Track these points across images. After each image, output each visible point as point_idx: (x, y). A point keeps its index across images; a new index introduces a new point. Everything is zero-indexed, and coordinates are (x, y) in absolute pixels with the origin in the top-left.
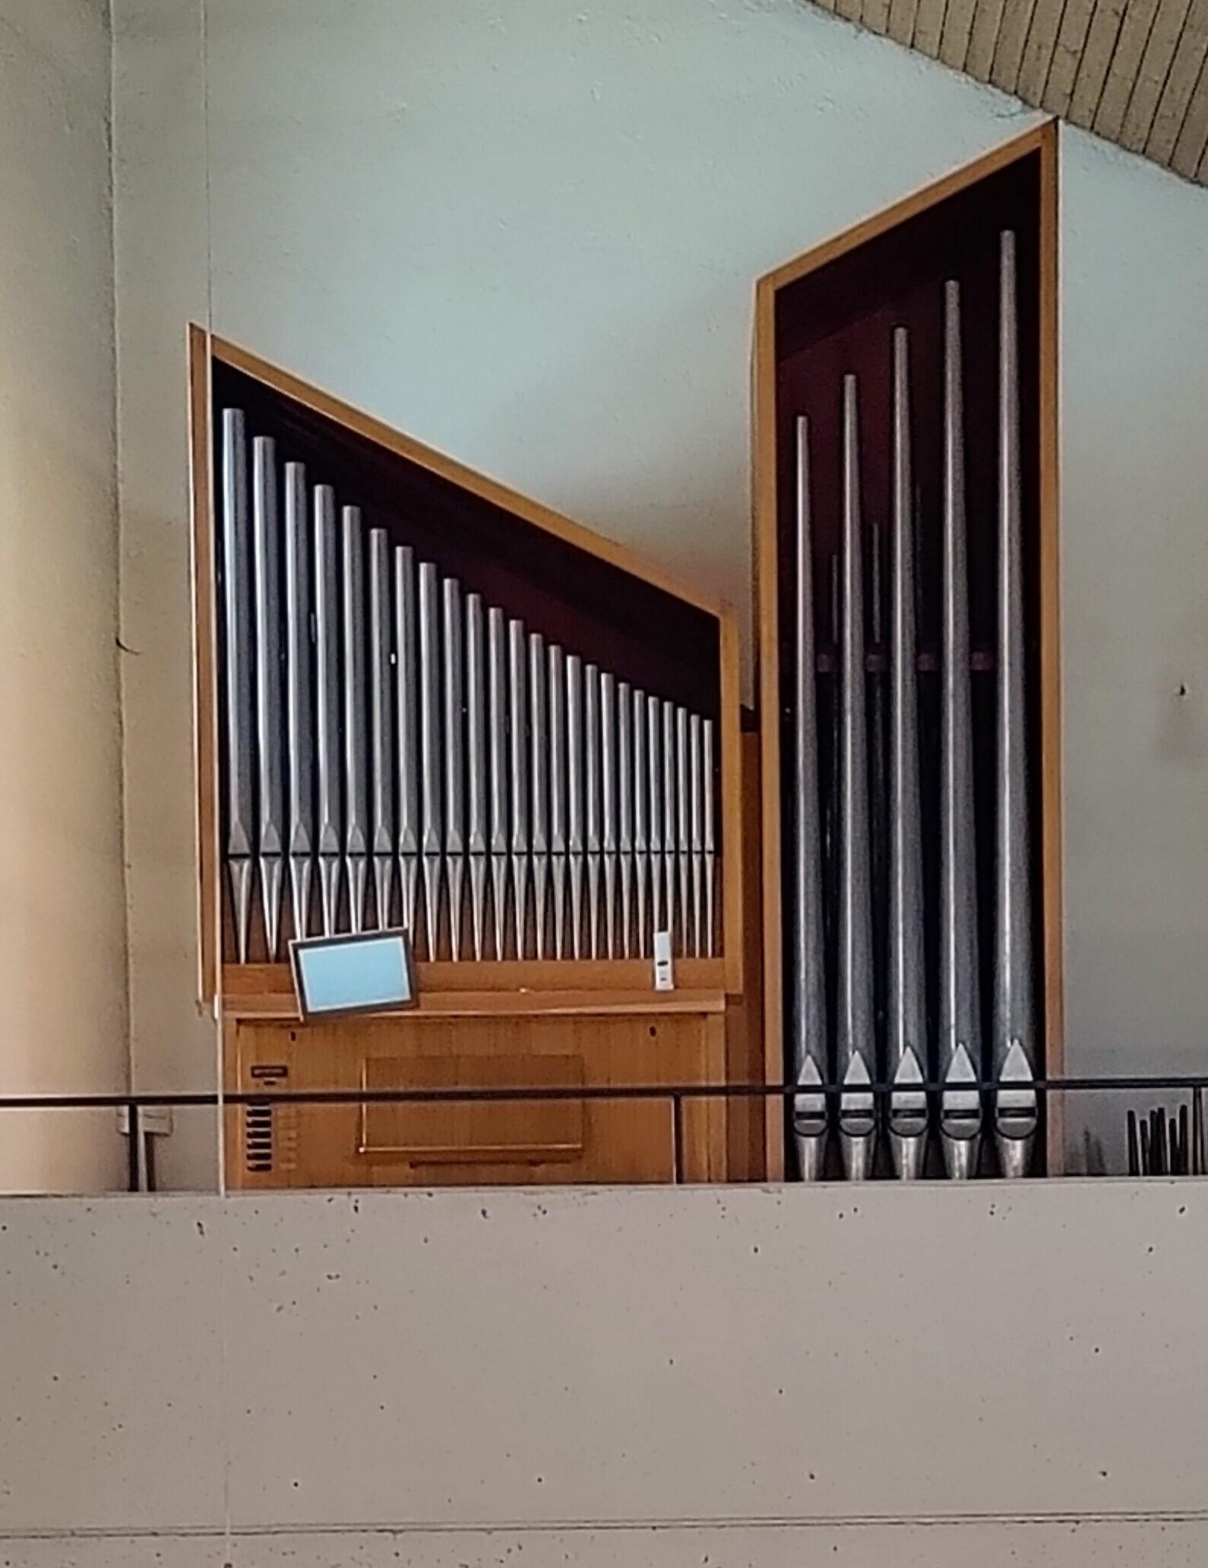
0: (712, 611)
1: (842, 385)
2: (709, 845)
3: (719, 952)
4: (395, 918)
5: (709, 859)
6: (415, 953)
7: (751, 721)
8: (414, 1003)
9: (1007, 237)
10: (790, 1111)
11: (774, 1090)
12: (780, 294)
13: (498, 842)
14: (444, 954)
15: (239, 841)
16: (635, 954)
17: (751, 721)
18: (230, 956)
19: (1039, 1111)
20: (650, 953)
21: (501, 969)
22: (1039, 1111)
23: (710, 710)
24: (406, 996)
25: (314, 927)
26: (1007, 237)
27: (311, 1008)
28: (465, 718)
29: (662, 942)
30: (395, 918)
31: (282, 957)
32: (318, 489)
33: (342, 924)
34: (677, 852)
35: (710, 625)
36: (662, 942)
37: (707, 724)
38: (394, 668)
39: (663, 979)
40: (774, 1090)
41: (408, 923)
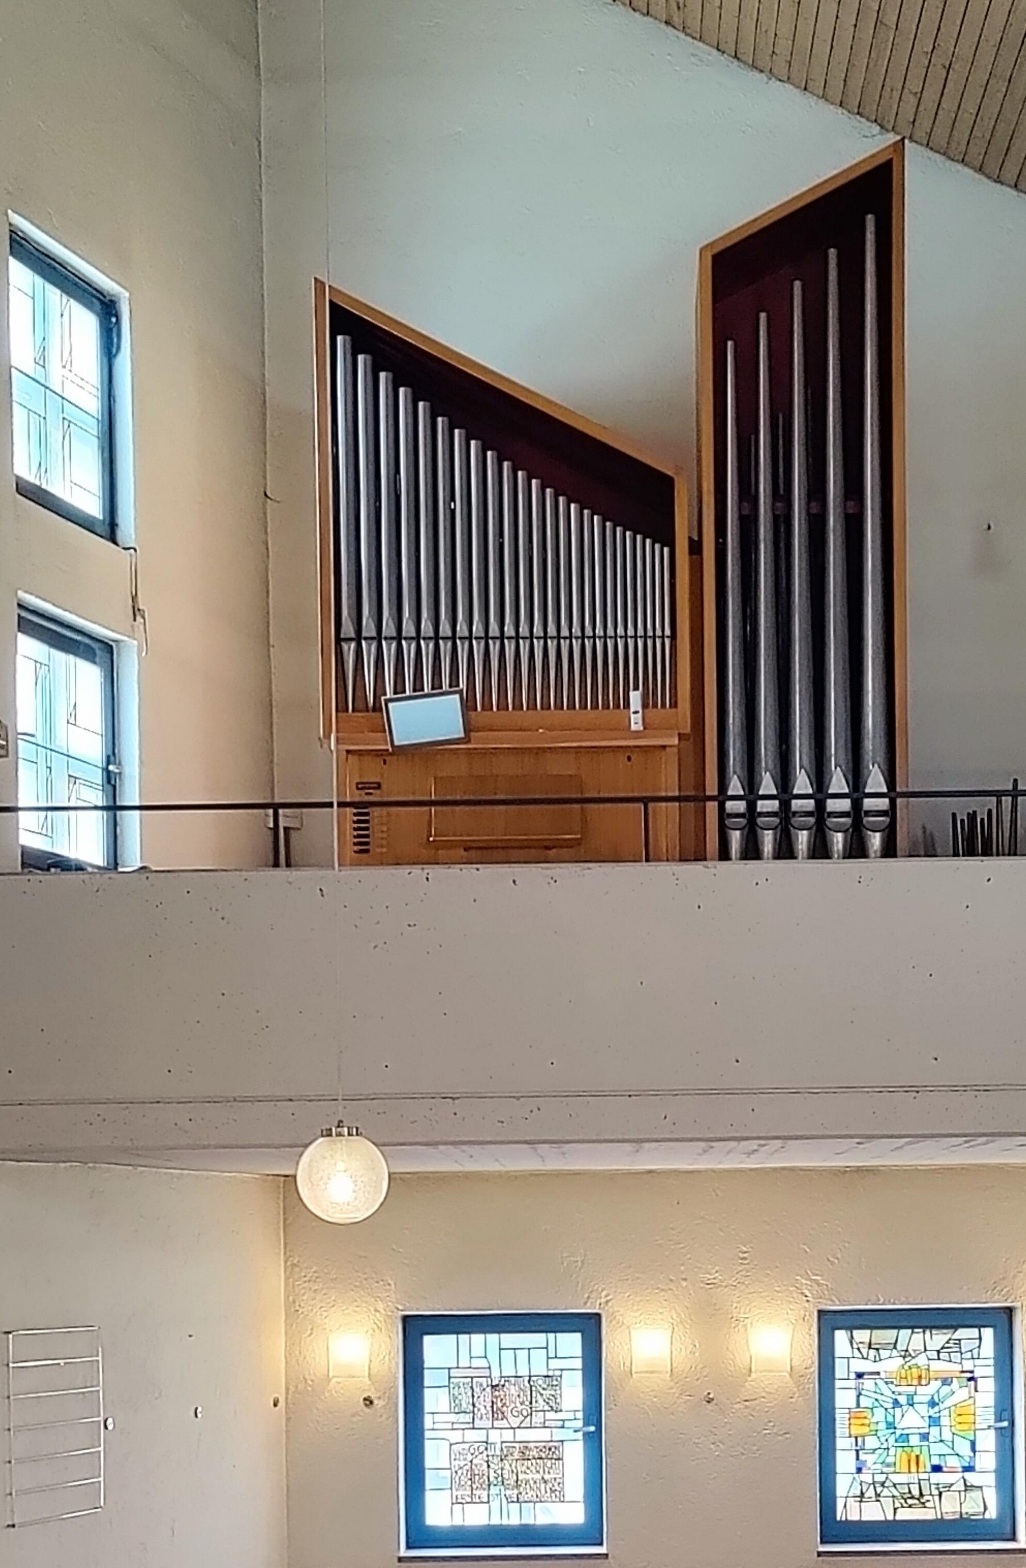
0: (670, 473)
1: (758, 319)
2: (668, 632)
3: (674, 704)
4: (454, 681)
5: (667, 641)
6: (468, 705)
7: (695, 548)
8: (467, 739)
9: (870, 219)
10: (722, 814)
11: (712, 798)
12: (716, 258)
13: (524, 630)
14: (487, 706)
15: (348, 629)
16: (617, 706)
17: (695, 548)
18: (342, 707)
19: (891, 812)
20: (627, 705)
21: (526, 716)
22: (891, 812)
23: (668, 539)
24: (462, 735)
25: (399, 688)
26: (870, 219)
27: (397, 743)
28: (501, 546)
29: (635, 698)
30: (454, 681)
31: (377, 708)
32: (402, 390)
33: (418, 686)
34: (645, 637)
35: (668, 482)
36: (635, 698)
37: (666, 550)
38: (453, 512)
39: (636, 723)
40: (712, 798)
41: (463, 685)
